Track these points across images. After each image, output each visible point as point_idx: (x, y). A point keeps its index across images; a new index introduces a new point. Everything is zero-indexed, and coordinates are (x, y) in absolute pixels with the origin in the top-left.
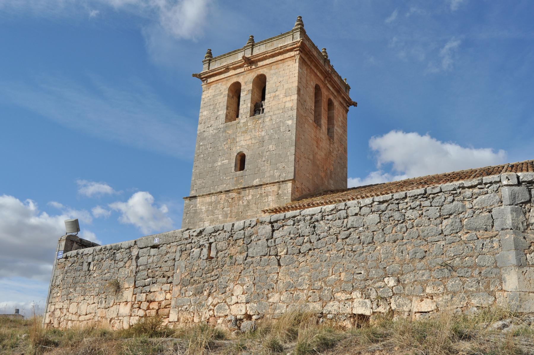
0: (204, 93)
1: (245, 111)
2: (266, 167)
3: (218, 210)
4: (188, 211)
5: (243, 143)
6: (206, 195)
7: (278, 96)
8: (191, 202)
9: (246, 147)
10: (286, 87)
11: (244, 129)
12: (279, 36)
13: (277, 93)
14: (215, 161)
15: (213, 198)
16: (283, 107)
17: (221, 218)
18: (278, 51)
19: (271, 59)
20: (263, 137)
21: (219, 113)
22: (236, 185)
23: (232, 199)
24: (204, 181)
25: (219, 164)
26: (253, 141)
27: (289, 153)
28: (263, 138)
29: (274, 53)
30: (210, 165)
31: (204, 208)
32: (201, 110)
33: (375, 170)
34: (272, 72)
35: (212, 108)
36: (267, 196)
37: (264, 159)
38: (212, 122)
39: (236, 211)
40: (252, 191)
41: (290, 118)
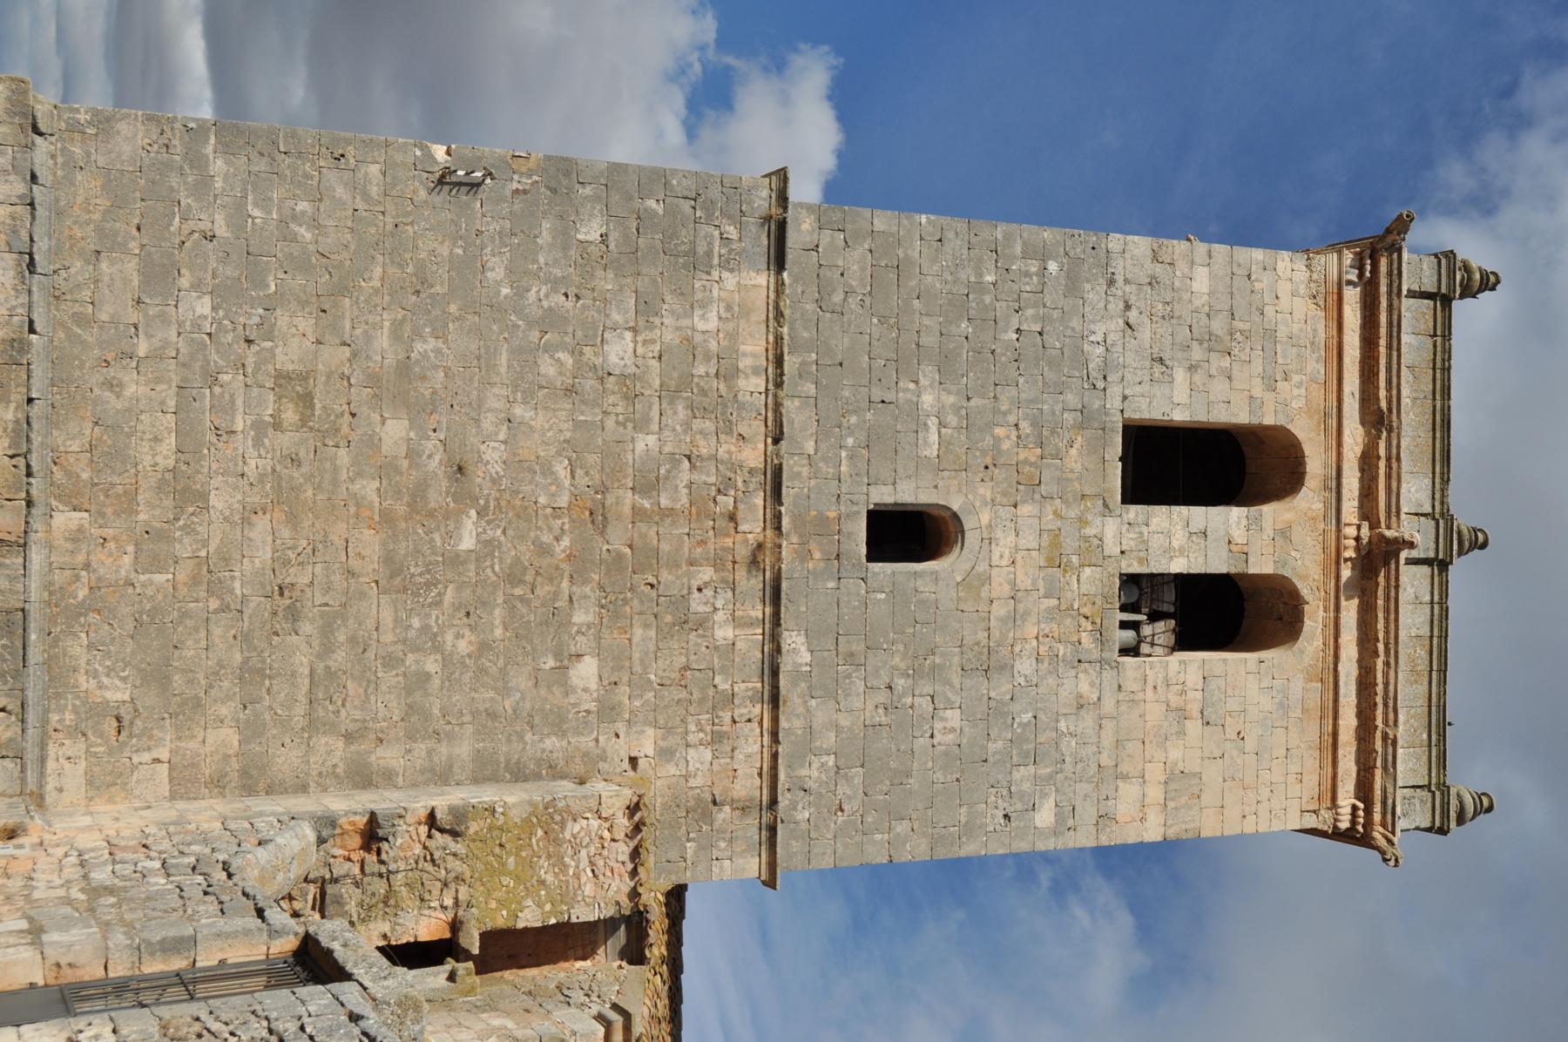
0: (1300, 262)
1: (1156, 542)
2: (858, 704)
3: (687, 426)
4: (709, 207)
5: (1002, 544)
6: (779, 339)
7: (1182, 733)
8: (752, 222)
9: (982, 567)
10: (1212, 773)
11: (1070, 543)
12: (1442, 709)
13: (1194, 727)
14: (946, 367)
15: (753, 385)
16: (1124, 768)
17: (640, 447)
18: (1379, 722)
19: (1354, 722)
20: (1007, 668)
21: (1180, 375)
22: (798, 520)
23: (732, 518)
24: (853, 302)
25: (928, 399)
26: (999, 610)
27: (901, 828)
28: (1002, 668)
29: (1379, 699)
30: (929, 340)
31: (707, 322)
32: (1220, 250)
33: (723, 43)
34: (1297, 686)
35: (1219, 326)
36: (717, 738)
37: (900, 683)
38: (1145, 334)
39: (665, 547)
40: (750, 642)
41: (1066, 816)
